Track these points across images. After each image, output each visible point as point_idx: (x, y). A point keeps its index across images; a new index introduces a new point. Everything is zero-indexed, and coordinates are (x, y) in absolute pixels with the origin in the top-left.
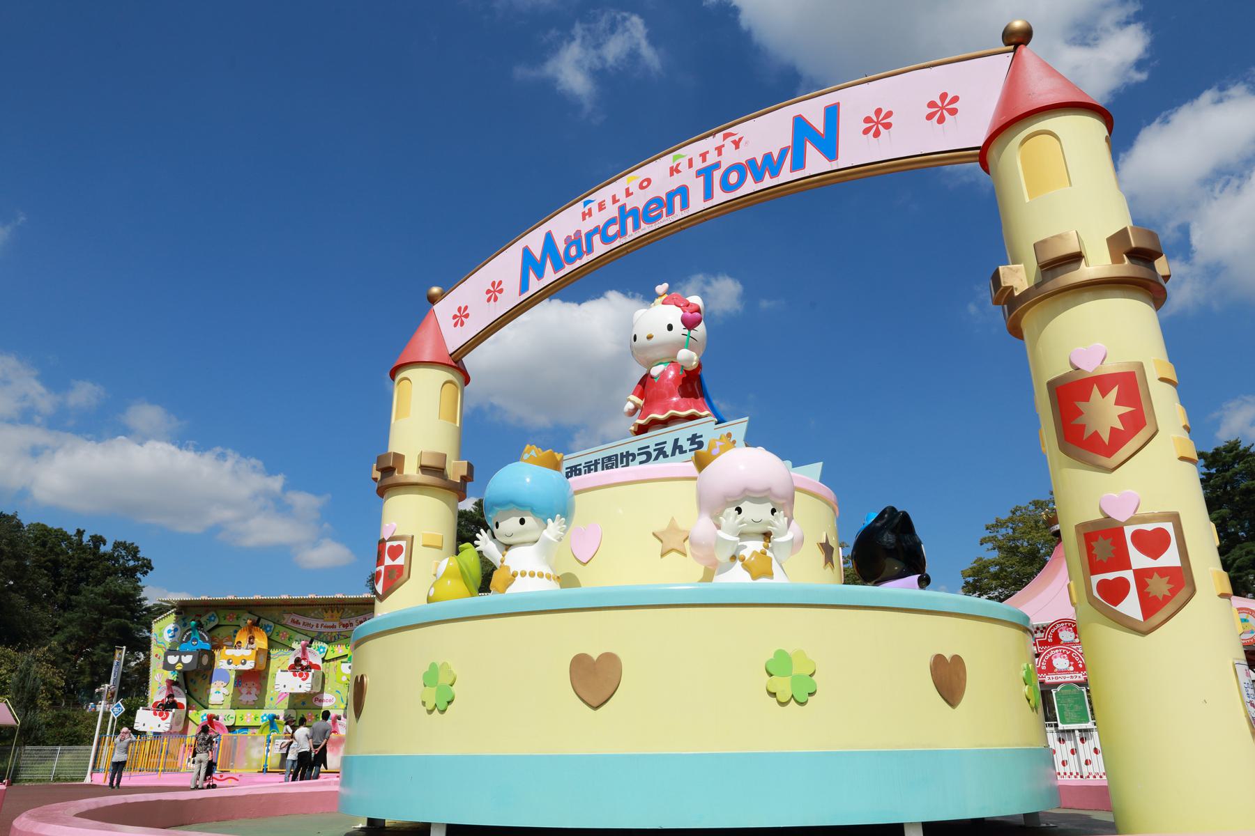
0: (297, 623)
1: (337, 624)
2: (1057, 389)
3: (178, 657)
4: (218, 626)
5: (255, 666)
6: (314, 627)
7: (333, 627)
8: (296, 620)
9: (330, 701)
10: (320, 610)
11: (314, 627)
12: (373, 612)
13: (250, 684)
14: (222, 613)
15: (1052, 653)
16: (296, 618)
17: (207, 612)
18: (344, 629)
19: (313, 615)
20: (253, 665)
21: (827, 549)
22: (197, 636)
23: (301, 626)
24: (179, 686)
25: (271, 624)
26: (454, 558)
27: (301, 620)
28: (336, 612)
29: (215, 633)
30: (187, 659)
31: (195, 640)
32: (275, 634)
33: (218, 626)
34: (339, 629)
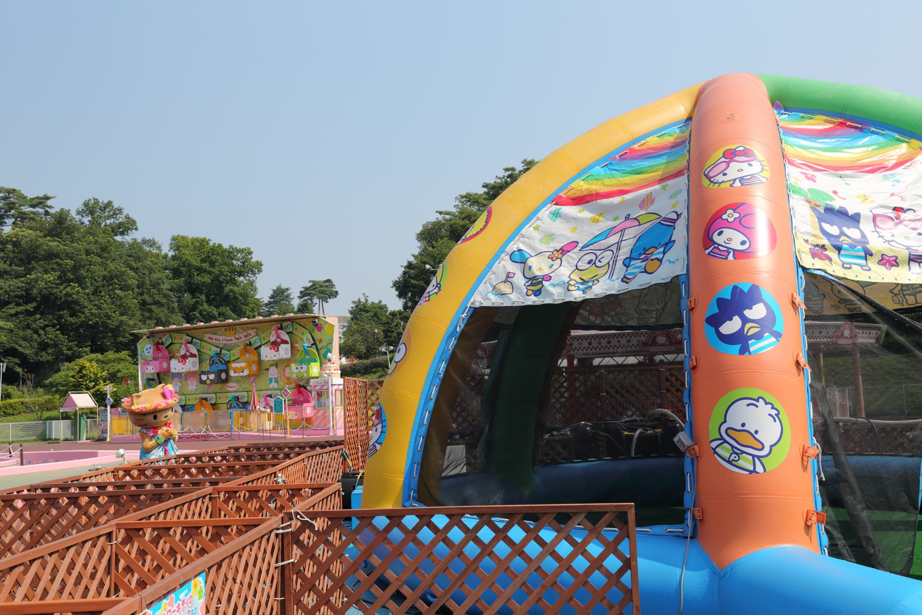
0: (212, 339)
1: (233, 338)
4: (171, 344)
5: (250, 372)
7: (231, 340)
9: (235, 387)
13: (192, 379)
14: (174, 335)
16: (211, 336)
17: (164, 335)
20: (248, 372)
23: (214, 341)
29: (170, 348)
34: (235, 341)
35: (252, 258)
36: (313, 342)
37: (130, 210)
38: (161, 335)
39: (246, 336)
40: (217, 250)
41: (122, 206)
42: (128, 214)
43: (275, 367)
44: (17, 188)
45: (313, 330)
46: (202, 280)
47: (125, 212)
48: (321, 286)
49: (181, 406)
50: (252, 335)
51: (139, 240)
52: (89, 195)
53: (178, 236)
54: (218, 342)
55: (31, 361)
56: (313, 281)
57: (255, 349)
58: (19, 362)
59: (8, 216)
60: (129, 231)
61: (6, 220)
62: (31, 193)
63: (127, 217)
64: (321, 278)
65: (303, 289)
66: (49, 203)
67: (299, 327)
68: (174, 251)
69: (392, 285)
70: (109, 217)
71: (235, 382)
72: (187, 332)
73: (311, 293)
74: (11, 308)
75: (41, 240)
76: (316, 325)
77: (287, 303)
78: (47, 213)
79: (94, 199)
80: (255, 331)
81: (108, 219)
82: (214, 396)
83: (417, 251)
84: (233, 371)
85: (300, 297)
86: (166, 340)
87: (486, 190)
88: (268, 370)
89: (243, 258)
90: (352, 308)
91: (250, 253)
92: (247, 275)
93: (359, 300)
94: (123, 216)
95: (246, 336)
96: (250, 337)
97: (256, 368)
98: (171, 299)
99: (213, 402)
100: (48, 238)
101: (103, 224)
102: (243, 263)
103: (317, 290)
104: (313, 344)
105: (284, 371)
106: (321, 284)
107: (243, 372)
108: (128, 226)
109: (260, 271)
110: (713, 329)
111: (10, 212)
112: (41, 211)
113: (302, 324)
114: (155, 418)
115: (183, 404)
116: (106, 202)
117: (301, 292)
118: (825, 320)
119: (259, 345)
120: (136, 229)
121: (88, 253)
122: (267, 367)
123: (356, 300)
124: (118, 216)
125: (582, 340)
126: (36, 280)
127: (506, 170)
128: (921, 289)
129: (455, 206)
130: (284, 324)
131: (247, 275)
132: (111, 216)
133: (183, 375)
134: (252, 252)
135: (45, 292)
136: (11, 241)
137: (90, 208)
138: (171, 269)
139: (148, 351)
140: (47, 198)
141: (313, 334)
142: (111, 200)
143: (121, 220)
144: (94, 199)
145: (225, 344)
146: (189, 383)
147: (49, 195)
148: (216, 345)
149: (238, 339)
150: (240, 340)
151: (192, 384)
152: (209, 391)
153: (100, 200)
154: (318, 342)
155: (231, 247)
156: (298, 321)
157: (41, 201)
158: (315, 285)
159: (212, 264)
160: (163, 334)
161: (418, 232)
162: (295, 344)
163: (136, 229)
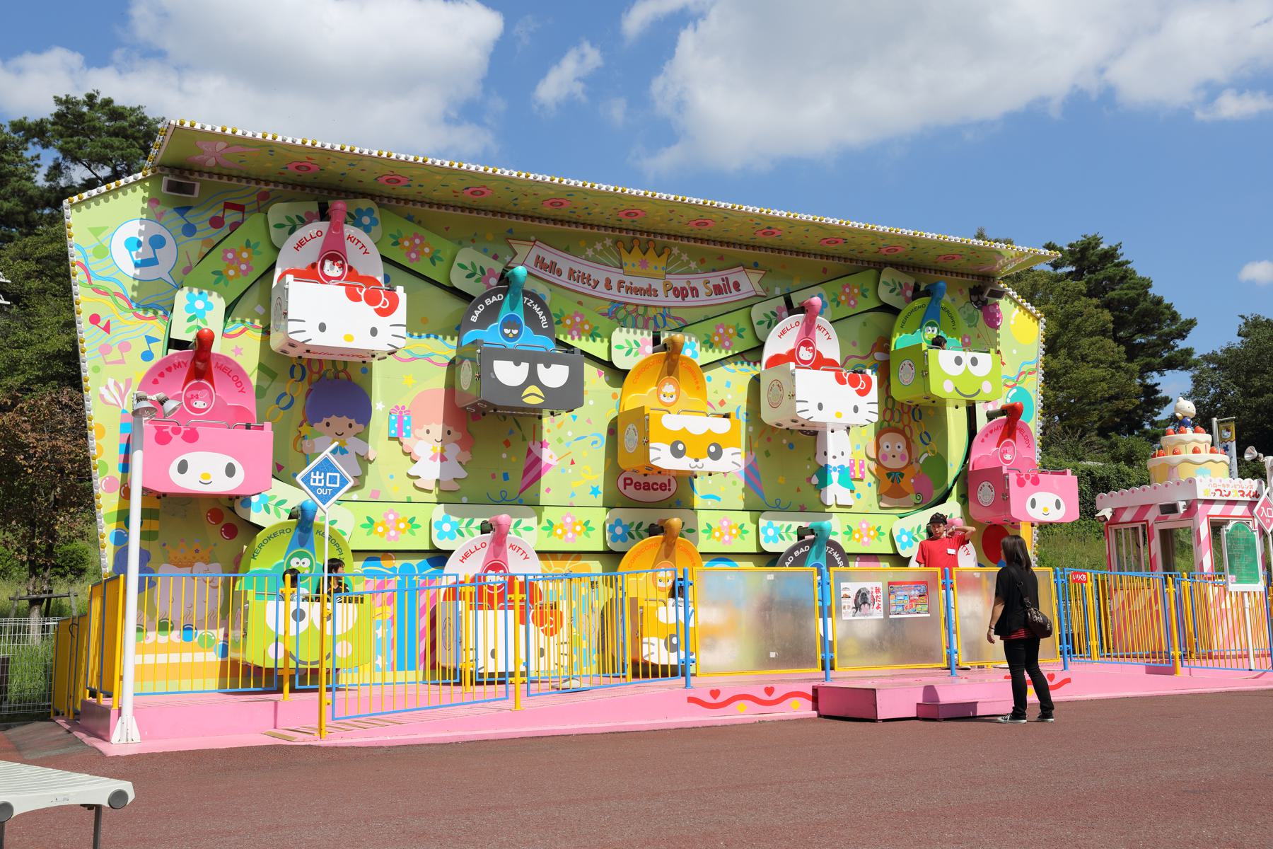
0: (552, 268)
2: (815, 433)
3: (525, 367)
6: (601, 287)
7: (650, 291)
8: (548, 261)
10: (608, 242)
11: (601, 287)
12: (1212, 528)
18: (678, 302)
19: (590, 252)
21: (936, 262)
22: (519, 313)
23: (563, 280)
31: (511, 322)
39: (718, 290)
84: (666, 449)
95: (718, 290)
97: (741, 460)
107: (716, 456)
110: (301, 419)
118: (1171, 627)
128: (1271, 344)
149: (681, 293)
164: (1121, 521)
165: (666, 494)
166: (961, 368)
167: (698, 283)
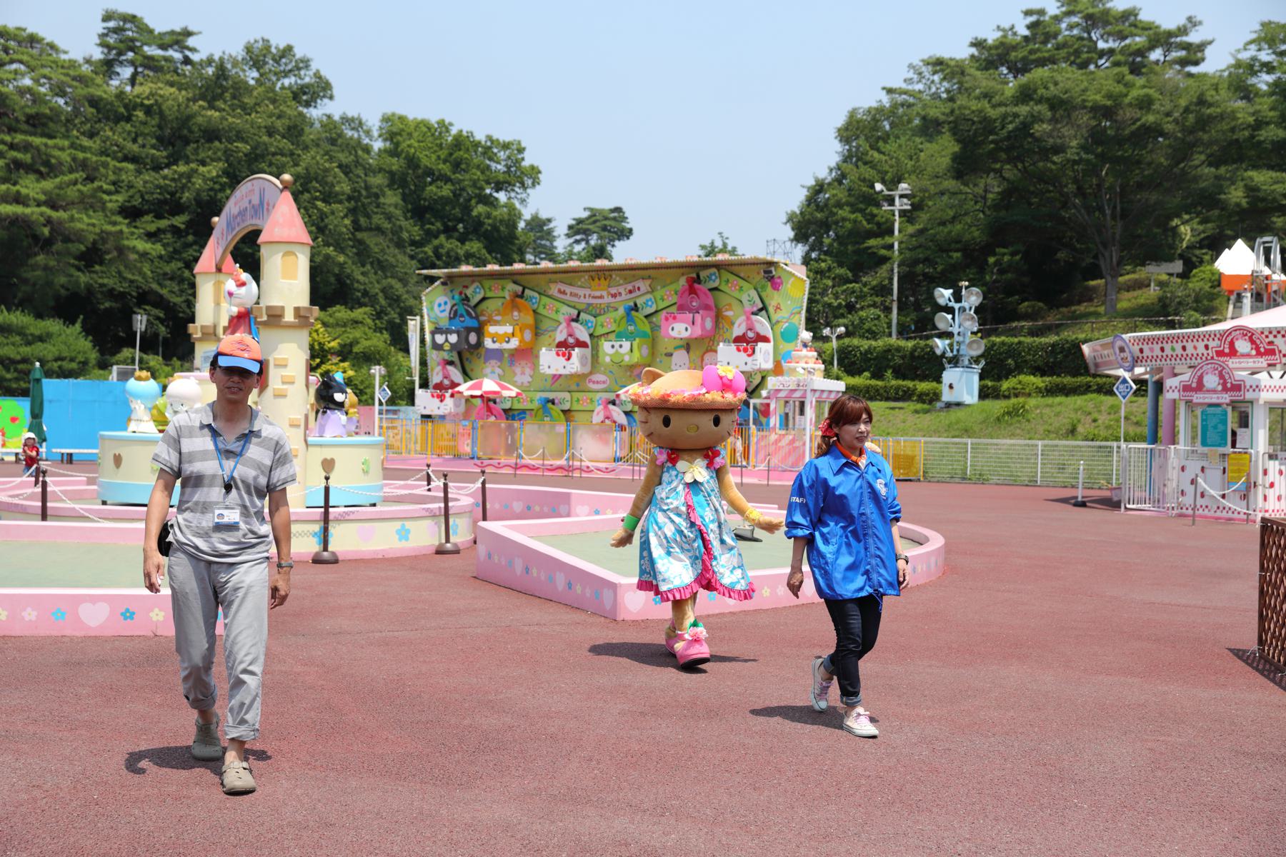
0: (564, 293)
1: (604, 294)
4: (484, 299)
7: (601, 297)
9: (604, 382)
13: (523, 363)
14: (487, 283)
15: (1205, 368)
16: (563, 287)
17: (473, 282)
23: (568, 297)
24: (455, 367)
25: (536, 295)
26: (198, 424)
27: (568, 289)
28: (603, 279)
30: (453, 338)
32: (541, 307)
33: (484, 299)
34: (609, 299)
35: (523, 159)
36: (760, 306)
37: (323, 64)
38: (467, 281)
39: (630, 292)
40: (462, 142)
41: (309, 55)
42: (318, 71)
43: (685, 352)
44: (139, 14)
45: (764, 288)
46: (440, 194)
47: (314, 66)
48: (606, 218)
49: (563, 411)
50: (643, 289)
51: (336, 118)
52: (253, 34)
53: (393, 115)
54: (575, 299)
55: (181, 315)
56: (591, 209)
57: (646, 317)
58: (162, 315)
59: (121, 63)
60: (319, 101)
61: (118, 69)
62: (160, 23)
63: (317, 75)
64: (605, 204)
65: (574, 222)
66: (191, 42)
67: (732, 278)
68: (385, 140)
69: (785, 220)
70: (286, 74)
71: (604, 373)
72: (518, 278)
73: (588, 230)
74: (147, 222)
75: (195, 107)
76: (771, 279)
77: (548, 243)
78: (187, 61)
79: (263, 40)
80: (648, 282)
81: (286, 76)
82: (567, 396)
83: (834, 159)
85: (568, 236)
86: (475, 294)
87: (974, 51)
88: (671, 355)
89: (509, 158)
90: (699, 256)
91: (521, 150)
92: (513, 190)
93: (713, 243)
94: (311, 73)
95: (630, 292)
96: (638, 293)
98: (398, 223)
99: (566, 406)
100: (201, 103)
101: (279, 85)
102: (509, 167)
103: (598, 224)
104: (761, 310)
105: (702, 360)
106: (606, 214)
108: (320, 89)
109: (536, 182)
111: (125, 54)
112: (177, 56)
113: (742, 275)
114: (717, 422)
115: (628, 409)
116: (282, 46)
117: (570, 227)
119: (653, 310)
120: (331, 98)
121: (271, 132)
122: (670, 350)
123: (707, 243)
124: (302, 72)
125: (1275, 336)
126: (189, 176)
127: (1028, 13)
129: (905, 81)
130: (703, 274)
131: (513, 190)
132: (290, 71)
133: (506, 355)
134: (524, 149)
135: (204, 196)
136: (142, 105)
137: (258, 56)
138: (387, 172)
139: (443, 307)
140: (187, 33)
141: (763, 294)
142: (292, 43)
143: (307, 80)
144: (263, 40)
145: (589, 305)
146: (518, 370)
147: (191, 28)
148: (573, 304)
149: (614, 296)
150: (618, 298)
151: (523, 373)
152: (553, 388)
153: (273, 43)
154: (771, 310)
155: (489, 138)
156: (736, 269)
157: (179, 39)
158: (595, 215)
159: (457, 166)
160: (471, 279)
161: (839, 125)
162: (727, 310)
163: (331, 98)
164: (170, 631)
165: (604, 386)
166: (614, 350)
167: (621, 290)
